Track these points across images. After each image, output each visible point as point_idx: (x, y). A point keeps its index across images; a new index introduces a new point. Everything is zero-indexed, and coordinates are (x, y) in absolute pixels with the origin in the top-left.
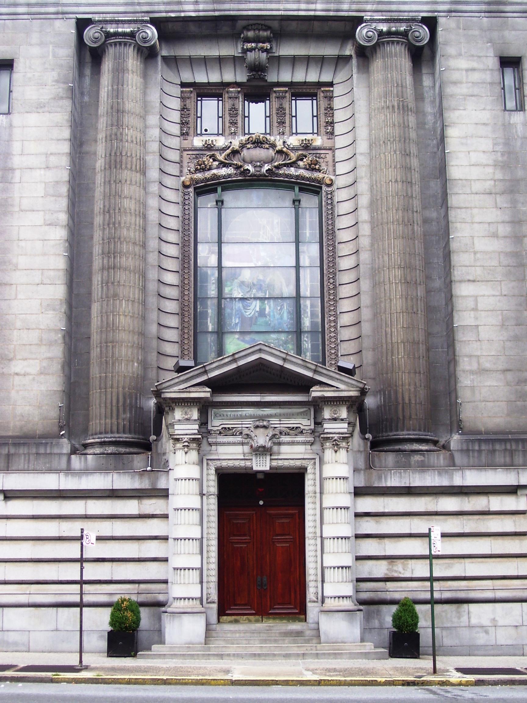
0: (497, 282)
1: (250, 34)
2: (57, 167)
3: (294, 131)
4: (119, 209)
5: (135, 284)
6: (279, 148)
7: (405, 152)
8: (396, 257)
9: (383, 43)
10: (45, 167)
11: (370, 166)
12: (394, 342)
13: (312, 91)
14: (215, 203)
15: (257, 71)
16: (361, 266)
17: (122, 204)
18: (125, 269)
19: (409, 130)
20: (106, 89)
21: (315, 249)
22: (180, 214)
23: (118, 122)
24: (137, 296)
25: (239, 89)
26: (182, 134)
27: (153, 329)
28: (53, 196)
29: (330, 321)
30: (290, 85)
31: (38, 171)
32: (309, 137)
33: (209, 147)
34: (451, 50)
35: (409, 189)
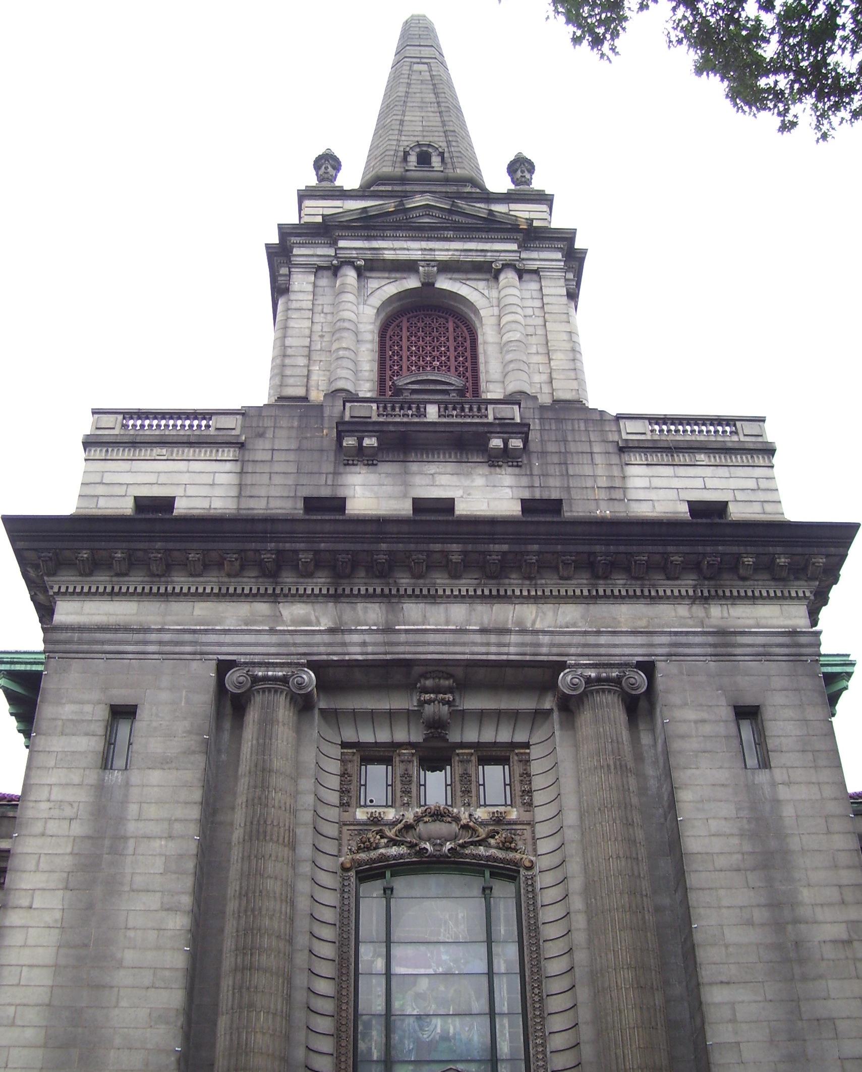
0: (759, 984)
1: (429, 683)
2: (182, 837)
3: (482, 803)
4: (261, 892)
5: (278, 990)
6: (464, 822)
7: (627, 820)
8: (625, 954)
9: (592, 692)
10: (166, 835)
11: (582, 841)
12: (628, 1067)
13: (503, 754)
14: (382, 892)
15: (437, 728)
16: (576, 969)
17: (265, 885)
18: (265, 971)
19: (629, 795)
20: (250, 743)
21: (512, 951)
22: (337, 904)
23: (263, 783)
24: (279, 1007)
25: (414, 751)
26: (342, 805)
27: (300, 1054)
28: (175, 873)
29: (536, 1045)
30: (477, 746)
31: (158, 841)
32: (501, 809)
33: (375, 821)
34: (675, 699)
35: (635, 867)
